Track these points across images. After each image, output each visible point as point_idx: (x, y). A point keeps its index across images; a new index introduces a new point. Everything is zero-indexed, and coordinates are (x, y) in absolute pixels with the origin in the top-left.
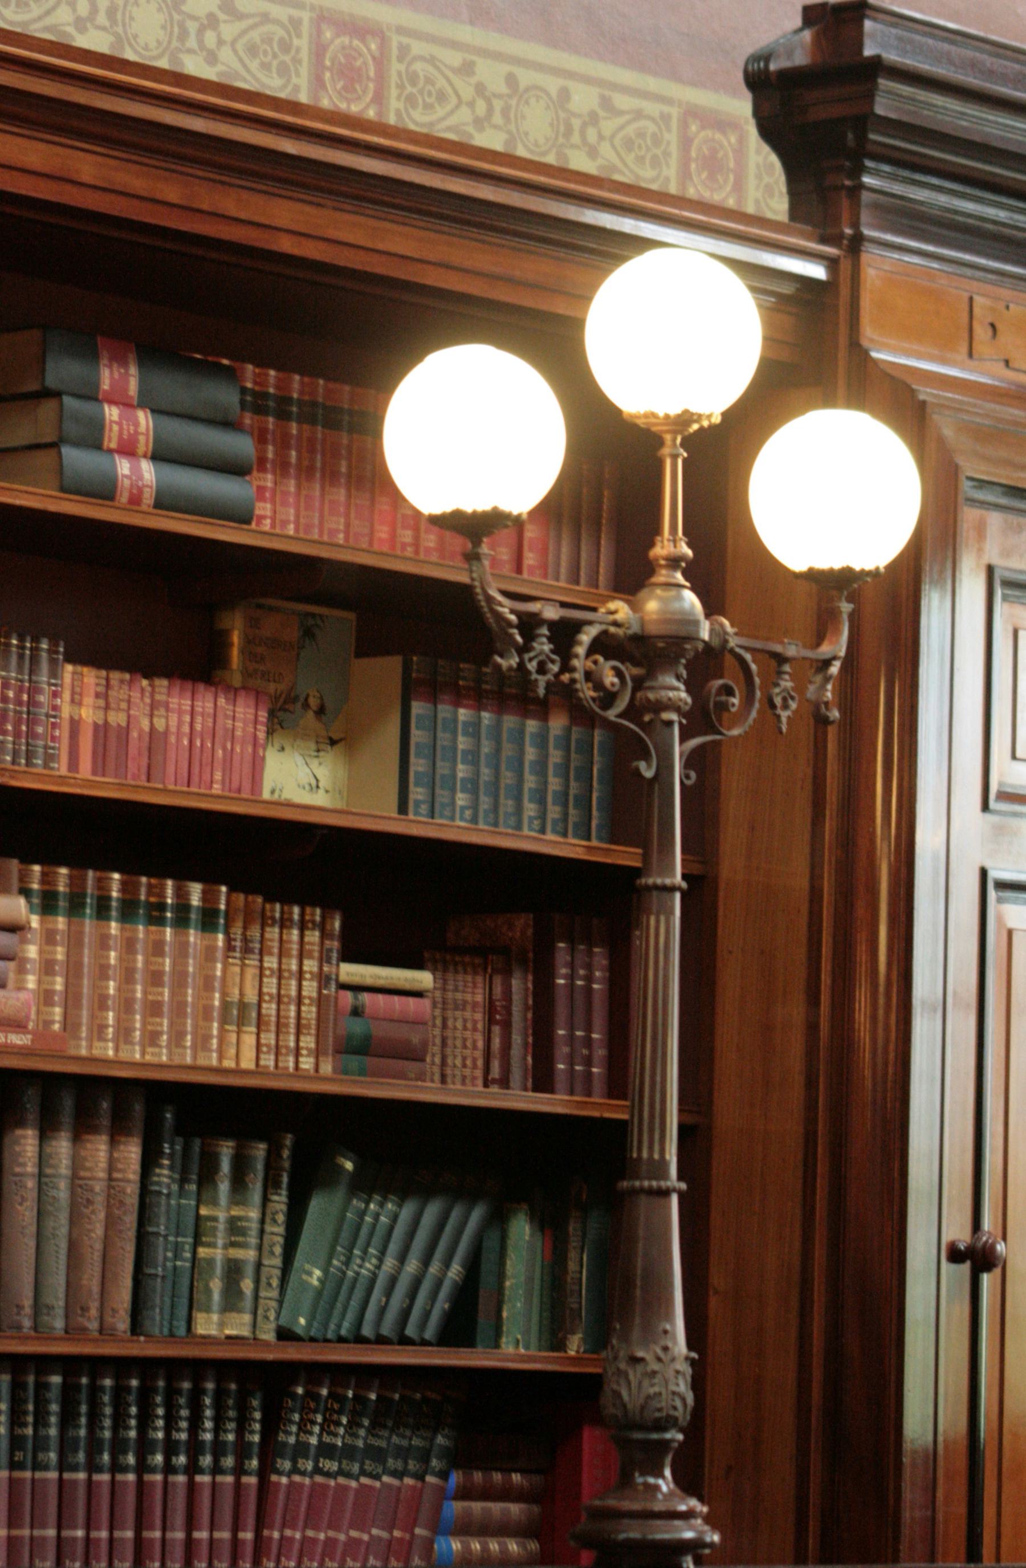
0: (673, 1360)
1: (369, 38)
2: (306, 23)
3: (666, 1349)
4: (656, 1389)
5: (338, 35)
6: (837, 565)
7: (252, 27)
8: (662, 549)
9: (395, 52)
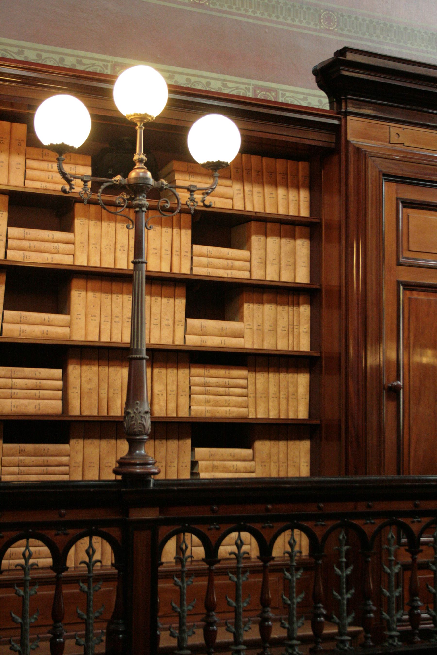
0: (140, 412)
1: (272, 92)
2: (251, 89)
3: (137, 409)
4: (134, 422)
5: (261, 91)
6: (215, 160)
7: (234, 90)
8: (136, 157)
9: (280, 95)
